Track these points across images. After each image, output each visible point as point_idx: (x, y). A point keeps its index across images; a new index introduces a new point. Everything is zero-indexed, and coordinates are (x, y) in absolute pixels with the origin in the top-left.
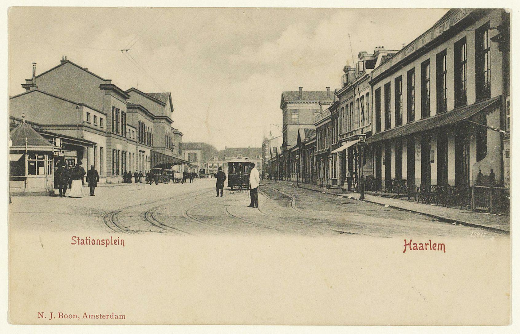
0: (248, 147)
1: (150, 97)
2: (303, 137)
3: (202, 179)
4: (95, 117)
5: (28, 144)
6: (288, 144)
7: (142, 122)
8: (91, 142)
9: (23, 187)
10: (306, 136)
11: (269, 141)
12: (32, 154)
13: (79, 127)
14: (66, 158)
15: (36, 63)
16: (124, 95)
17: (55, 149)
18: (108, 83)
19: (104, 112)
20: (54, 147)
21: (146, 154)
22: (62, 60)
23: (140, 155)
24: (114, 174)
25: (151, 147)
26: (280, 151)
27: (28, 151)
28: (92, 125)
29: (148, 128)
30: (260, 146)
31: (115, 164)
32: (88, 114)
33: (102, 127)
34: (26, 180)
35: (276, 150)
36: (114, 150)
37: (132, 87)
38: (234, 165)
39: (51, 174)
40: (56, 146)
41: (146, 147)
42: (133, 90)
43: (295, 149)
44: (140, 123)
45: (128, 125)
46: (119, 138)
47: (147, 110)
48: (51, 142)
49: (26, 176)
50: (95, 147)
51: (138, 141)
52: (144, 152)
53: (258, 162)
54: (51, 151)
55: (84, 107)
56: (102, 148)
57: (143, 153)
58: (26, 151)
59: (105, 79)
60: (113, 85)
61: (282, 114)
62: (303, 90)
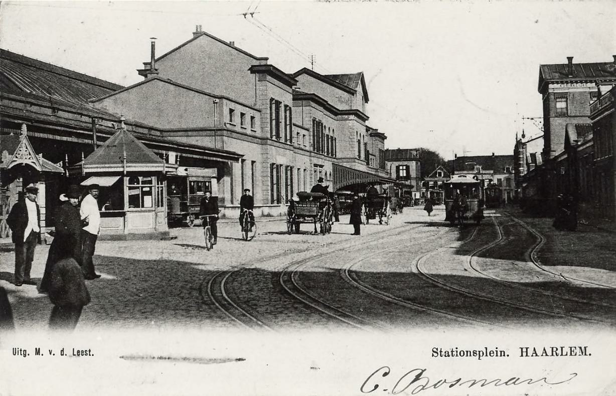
0: (492, 155)
1: (332, 80)
2: (573, 137)
3: (405, 209)
4: (242, 115)
5: (127, 162)
6: (552, 149)
7: (317, 120)
8: (234, 153)
9: (122, 227)
10: (579, 134)
11: (524, 144)
12: (134, 177)
13: (216, 132)
14: (191, 179)
15: (156, 39)
16: (288, 80)
17: (166, 167)
18: (263, 63)
19: (257, 107)
20: (167, 165)
21: (323, 170)
22: (195, 31)
23: (315, 171)
24: (273, 202)
25: (334, 158)
26: (539, 159)
27: (127, 172)
28: (238, 129)
29: (327, 129)
30: (511, 152)
31: (275, 186)
32: (231, 111)
33: (245, 127)
34: (126, 216)
35: (533, 156)
36: (273, 164)
37: (303, 67)
38: (451, 186)
39: (162, 206)
40: (169, 163)
41: (325, 158)
42: (305, 71)
43: (563, 158)
44: (315, 122)
45: (295, 125)
46: (281, 145)
47: (327, 102)
48: (161, 156)
49: (125, 211)
50: (243, 161)
51: (312, 149)
52: (321, 166)
53: (128, 207)
54: (161, 172)
55: (225, 101)
56: (255, 162)
57: (321, 168)
58: (125, 172)
59: (258, 56)
60: (271, 66)
61: (542, 102)
62: (574, 62)
